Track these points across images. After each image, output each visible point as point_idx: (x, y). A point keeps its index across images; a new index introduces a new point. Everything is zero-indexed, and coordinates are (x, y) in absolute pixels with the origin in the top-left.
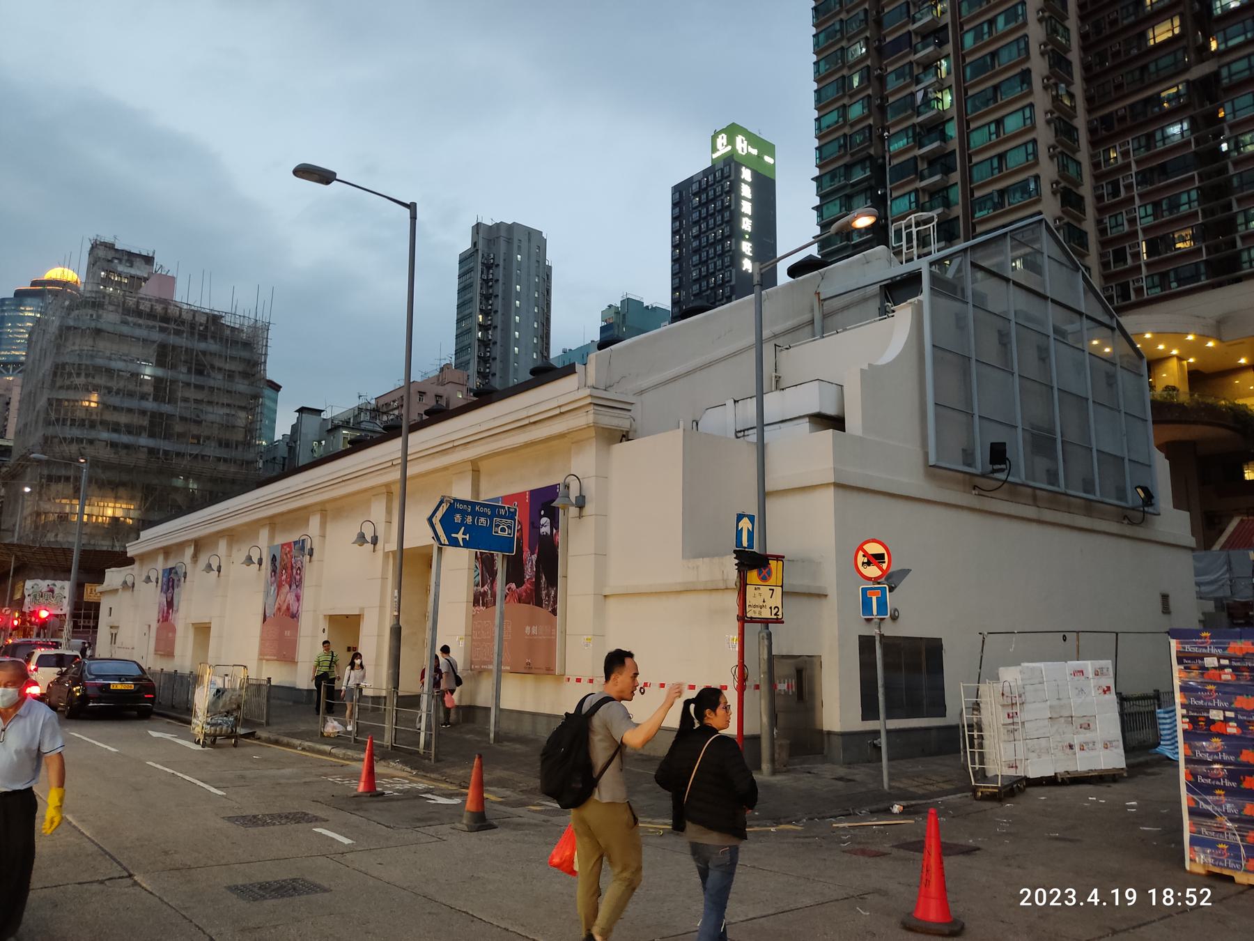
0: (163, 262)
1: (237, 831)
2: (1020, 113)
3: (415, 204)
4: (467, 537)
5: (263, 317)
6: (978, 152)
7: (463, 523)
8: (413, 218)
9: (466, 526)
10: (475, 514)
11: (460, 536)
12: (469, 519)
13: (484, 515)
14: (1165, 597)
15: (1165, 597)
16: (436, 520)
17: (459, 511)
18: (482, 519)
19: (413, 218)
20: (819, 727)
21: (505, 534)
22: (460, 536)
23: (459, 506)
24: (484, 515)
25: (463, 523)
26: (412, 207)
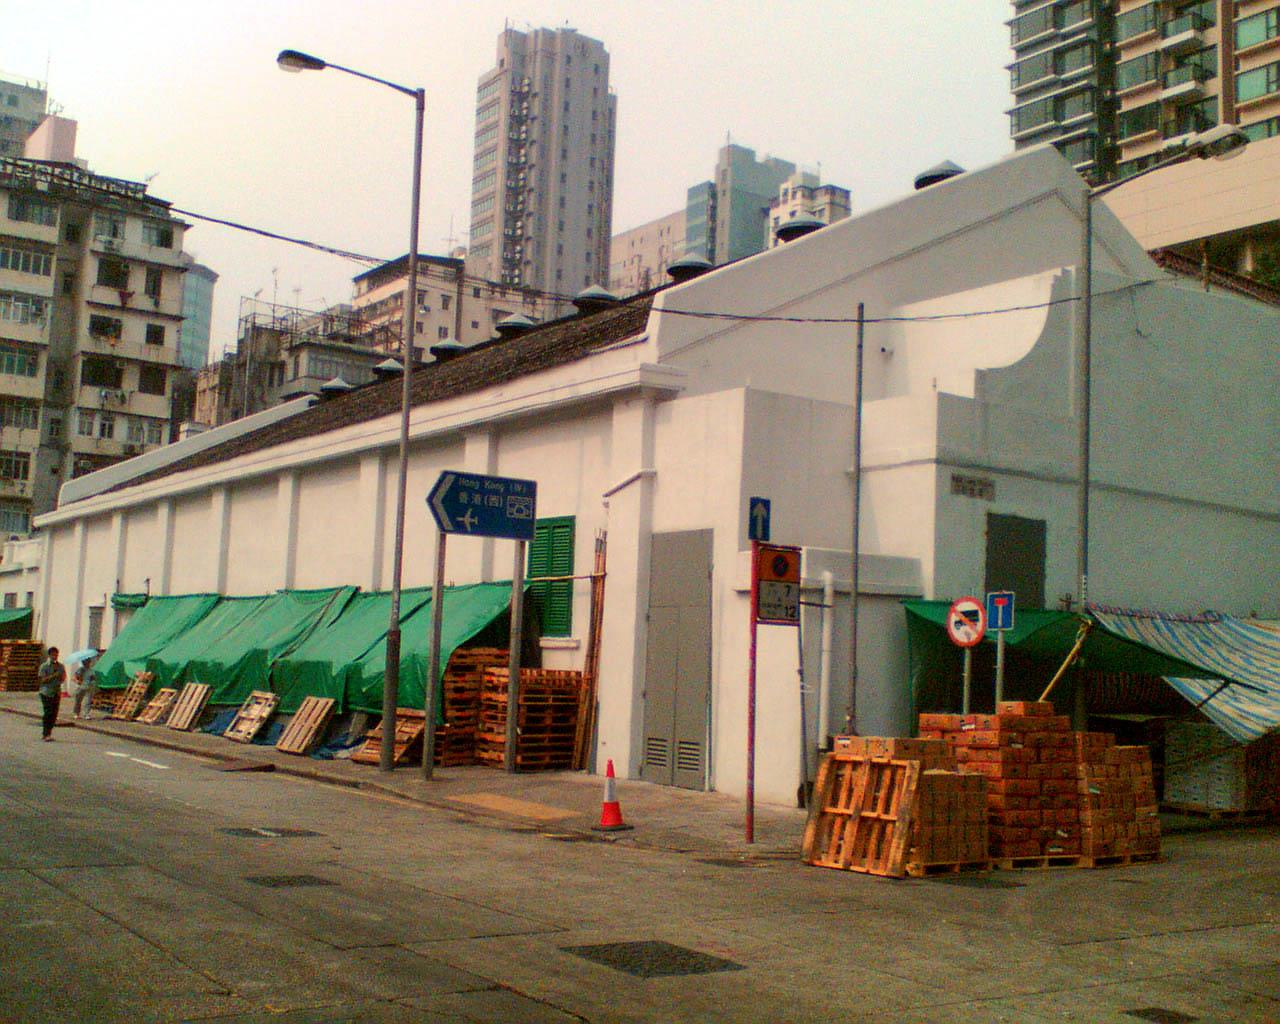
0: (61, 101)
1: (247, 885)
2: (1263, 19)
3: (422, 92)
4: (476, 521)
5: (76, 119)
6: (1249, 108)
7: (470, 503)
8: (421, 108)
9: (474, 506)
10: (483, 492)
11: (467, 520)
12: (477, 499)
13: (496, 492)
14: (935, 380)
15: (935, 380)
16: (437, 501)
17: (465, 489)
18: (494, 499)
19: (421, 108)
20: (362, 463)
21: (522, 516)
22: (467, 520)
23: (465, 482)
24: (496, 492)
25: (470, 503)
26: (419, 95)
